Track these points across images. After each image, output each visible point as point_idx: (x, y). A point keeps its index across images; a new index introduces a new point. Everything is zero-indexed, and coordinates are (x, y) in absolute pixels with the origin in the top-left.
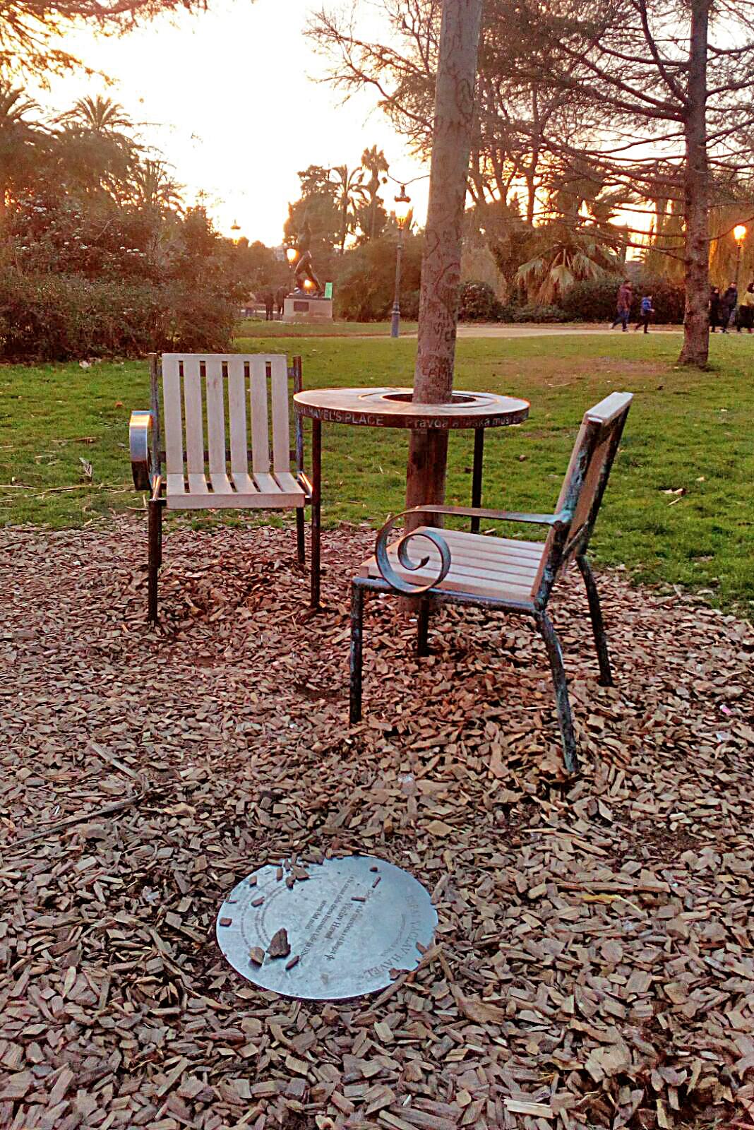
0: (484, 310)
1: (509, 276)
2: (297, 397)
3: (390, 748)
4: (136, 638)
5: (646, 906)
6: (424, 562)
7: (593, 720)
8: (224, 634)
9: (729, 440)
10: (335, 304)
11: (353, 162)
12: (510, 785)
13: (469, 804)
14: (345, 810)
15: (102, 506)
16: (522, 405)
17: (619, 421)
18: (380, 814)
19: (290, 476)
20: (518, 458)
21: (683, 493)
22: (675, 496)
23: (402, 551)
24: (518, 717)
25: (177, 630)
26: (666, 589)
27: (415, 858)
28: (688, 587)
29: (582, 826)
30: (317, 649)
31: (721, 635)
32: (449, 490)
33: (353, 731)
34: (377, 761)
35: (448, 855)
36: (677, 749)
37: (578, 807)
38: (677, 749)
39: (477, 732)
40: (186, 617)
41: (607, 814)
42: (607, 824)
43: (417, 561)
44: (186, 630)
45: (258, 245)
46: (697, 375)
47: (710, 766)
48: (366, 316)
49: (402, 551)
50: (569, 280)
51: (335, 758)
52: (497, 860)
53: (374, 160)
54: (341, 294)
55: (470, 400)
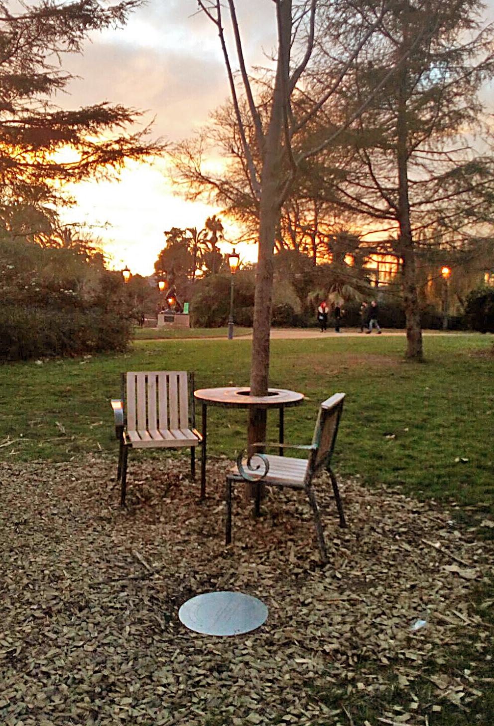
0: (287, 319)
1: (303, 297)
2: (197, 394)
3: (244, 554)
4: (116, 513)
5: (352, 605)
6: (258, 467)
7: (336, 541)
8: (159, 510)
9: (425, 407)
10: (191, 317)
11: (200, 226)
12: (298, 567)
13: (280, 574)
14: (227, 577)
15: (76, 449)
16: (300, 396)
17: (339, 406)
18: (241, 577)
19: (189, 431)
20: (307, 419)
21: (396, 437)
22: (390, 439)
23: (249, 464)
24: (302, 540)
25: (135, 509)
26: (379, 486)
27: (258, 593)
28: (390, 485)
29: (328, 580)
30: (206, 516)
31: (403, 507)
32: (268, 437)
33: (228, 547)
34: (239, 559)
35: (272, 591)
36: (374, 552)
37: (327, 574)
38: (374, 552)
39: (283, 545)
40: (138, 503)
41: (339, 576)
42: (339, 579)
43: (255, 468)
44: (139, 509)
45: (138, 275)
46: (416, 366)
47: (386, 558)
48: (210, 324)
49: (249, 464)
50: (341, 302)
51: (220, 559)
52: (292, 592)
53: (214, 225)
54: (195, 310)
55: (276, 394)
